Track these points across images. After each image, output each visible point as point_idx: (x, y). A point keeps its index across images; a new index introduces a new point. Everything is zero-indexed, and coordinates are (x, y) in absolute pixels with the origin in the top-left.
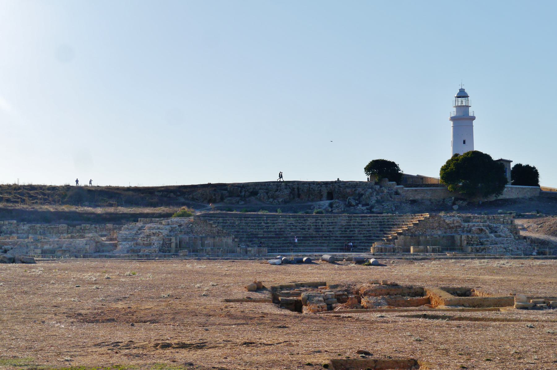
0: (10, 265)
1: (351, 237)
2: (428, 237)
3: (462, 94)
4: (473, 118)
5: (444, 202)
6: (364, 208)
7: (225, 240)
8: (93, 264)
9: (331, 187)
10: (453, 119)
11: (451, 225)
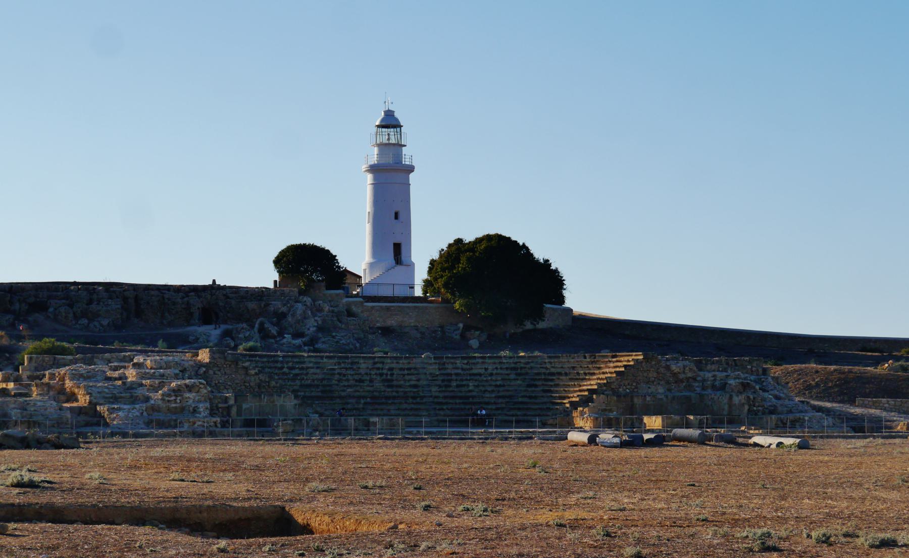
0: (237, 448)
1: (468, 398)
2: (648, 398)
3: (390, 122)
4: (411, 169)
5: (443, 332)
6: (298, 342)
7: (279, 401)
8: (157, 452)
9: (209, 297)
10: (373, 169)
11: (682, 376)
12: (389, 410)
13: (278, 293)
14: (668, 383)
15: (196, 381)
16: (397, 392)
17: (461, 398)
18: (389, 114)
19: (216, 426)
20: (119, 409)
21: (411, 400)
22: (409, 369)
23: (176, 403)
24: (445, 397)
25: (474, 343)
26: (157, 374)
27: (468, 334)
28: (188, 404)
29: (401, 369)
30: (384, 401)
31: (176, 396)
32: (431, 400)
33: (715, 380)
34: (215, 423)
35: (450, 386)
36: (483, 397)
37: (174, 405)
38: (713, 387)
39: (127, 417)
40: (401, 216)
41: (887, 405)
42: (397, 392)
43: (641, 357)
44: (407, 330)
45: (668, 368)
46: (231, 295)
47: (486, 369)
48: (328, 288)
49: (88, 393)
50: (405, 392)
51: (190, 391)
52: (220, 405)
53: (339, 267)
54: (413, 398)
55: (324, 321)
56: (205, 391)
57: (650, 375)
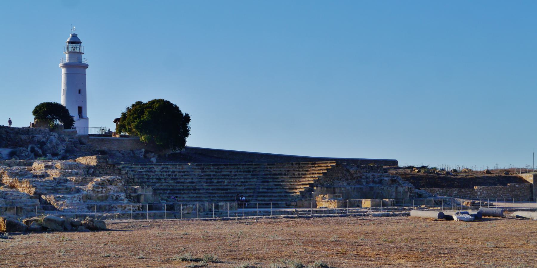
1: (227, 189)
2: (342, 189)
3: (75, 41)
4: (86, 66)
5: (134, 154)
10: (66, 66)
12: (183, 198)
13: (38, 131)
14: (347, 179)
15: (114, 177)
16: (183, 186)
17: (223, 189)
18: (74, 36)
19: (139, 209)
20: (64, 198)
21: (193, 191)
22: (184, 172)
23: (102, 193)
24: (213, 189)
25: (154, 160)
26: (73, 173)
27: (147, 155)
28: (110, 193)
29: (179, 172)
30: (177, 192)
31: (102, 188)
32: (204, 191)
33: (374, 178)
34: (138, 207)
35: (213, 182)
36: (236, 189)
37: (101, 195)
38: (374, 182)
39: (72, 204)
40: (82, 91)
41: (438, 192)
42: (183, 186)
43: (335, 164)
44: (114, 152)
45: (348, 171)
46: (10, 131)
47: (231, 172)
48: (65, 128)
49: (33, 187)
50: (188, 186)
51: (111, 184)
52: (133, 194)
53: (147, 104)
54: (195, 190)
55: (67, 146)
56: (121, 184)
57: (339, 175)
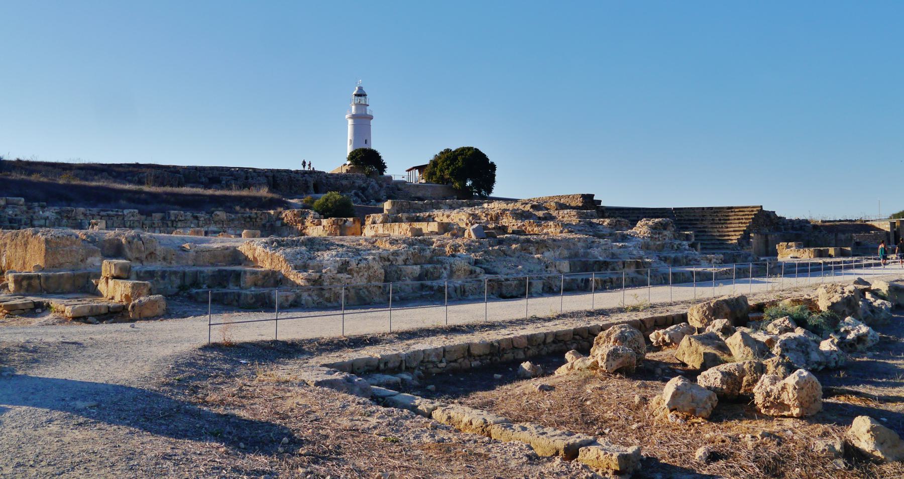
4: (371, 118)
10: (354, 117)
51: (665, 229)
